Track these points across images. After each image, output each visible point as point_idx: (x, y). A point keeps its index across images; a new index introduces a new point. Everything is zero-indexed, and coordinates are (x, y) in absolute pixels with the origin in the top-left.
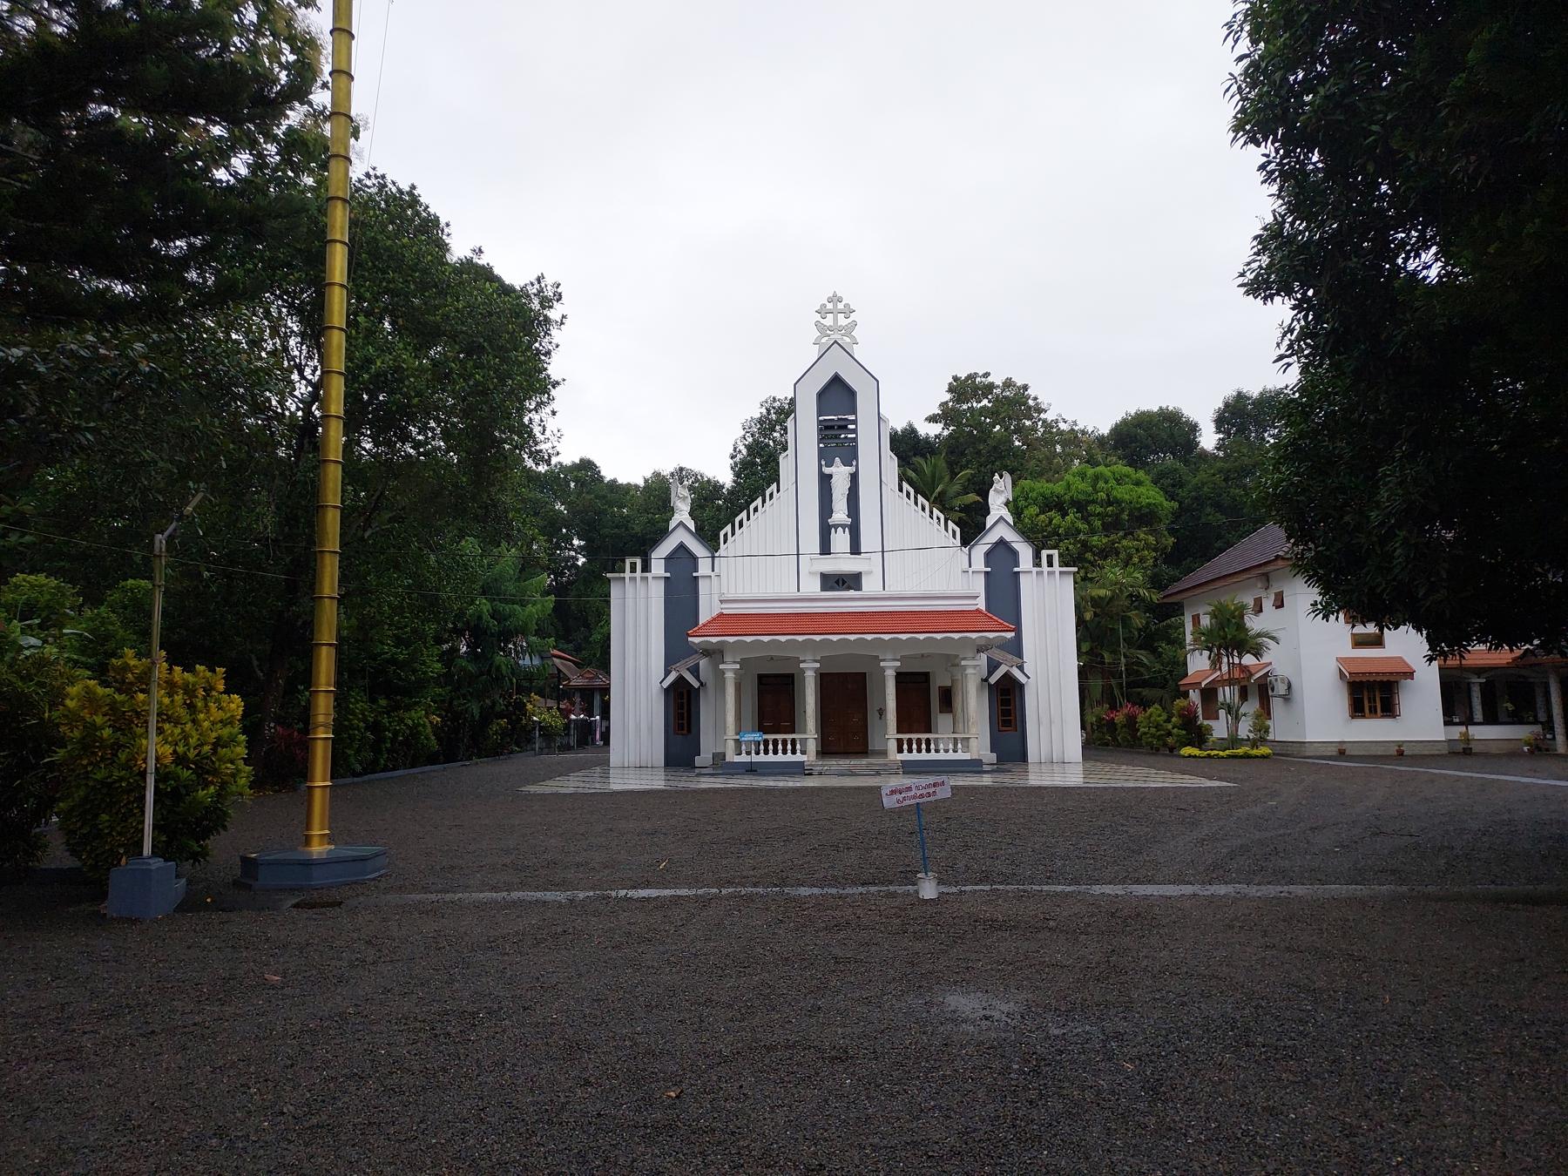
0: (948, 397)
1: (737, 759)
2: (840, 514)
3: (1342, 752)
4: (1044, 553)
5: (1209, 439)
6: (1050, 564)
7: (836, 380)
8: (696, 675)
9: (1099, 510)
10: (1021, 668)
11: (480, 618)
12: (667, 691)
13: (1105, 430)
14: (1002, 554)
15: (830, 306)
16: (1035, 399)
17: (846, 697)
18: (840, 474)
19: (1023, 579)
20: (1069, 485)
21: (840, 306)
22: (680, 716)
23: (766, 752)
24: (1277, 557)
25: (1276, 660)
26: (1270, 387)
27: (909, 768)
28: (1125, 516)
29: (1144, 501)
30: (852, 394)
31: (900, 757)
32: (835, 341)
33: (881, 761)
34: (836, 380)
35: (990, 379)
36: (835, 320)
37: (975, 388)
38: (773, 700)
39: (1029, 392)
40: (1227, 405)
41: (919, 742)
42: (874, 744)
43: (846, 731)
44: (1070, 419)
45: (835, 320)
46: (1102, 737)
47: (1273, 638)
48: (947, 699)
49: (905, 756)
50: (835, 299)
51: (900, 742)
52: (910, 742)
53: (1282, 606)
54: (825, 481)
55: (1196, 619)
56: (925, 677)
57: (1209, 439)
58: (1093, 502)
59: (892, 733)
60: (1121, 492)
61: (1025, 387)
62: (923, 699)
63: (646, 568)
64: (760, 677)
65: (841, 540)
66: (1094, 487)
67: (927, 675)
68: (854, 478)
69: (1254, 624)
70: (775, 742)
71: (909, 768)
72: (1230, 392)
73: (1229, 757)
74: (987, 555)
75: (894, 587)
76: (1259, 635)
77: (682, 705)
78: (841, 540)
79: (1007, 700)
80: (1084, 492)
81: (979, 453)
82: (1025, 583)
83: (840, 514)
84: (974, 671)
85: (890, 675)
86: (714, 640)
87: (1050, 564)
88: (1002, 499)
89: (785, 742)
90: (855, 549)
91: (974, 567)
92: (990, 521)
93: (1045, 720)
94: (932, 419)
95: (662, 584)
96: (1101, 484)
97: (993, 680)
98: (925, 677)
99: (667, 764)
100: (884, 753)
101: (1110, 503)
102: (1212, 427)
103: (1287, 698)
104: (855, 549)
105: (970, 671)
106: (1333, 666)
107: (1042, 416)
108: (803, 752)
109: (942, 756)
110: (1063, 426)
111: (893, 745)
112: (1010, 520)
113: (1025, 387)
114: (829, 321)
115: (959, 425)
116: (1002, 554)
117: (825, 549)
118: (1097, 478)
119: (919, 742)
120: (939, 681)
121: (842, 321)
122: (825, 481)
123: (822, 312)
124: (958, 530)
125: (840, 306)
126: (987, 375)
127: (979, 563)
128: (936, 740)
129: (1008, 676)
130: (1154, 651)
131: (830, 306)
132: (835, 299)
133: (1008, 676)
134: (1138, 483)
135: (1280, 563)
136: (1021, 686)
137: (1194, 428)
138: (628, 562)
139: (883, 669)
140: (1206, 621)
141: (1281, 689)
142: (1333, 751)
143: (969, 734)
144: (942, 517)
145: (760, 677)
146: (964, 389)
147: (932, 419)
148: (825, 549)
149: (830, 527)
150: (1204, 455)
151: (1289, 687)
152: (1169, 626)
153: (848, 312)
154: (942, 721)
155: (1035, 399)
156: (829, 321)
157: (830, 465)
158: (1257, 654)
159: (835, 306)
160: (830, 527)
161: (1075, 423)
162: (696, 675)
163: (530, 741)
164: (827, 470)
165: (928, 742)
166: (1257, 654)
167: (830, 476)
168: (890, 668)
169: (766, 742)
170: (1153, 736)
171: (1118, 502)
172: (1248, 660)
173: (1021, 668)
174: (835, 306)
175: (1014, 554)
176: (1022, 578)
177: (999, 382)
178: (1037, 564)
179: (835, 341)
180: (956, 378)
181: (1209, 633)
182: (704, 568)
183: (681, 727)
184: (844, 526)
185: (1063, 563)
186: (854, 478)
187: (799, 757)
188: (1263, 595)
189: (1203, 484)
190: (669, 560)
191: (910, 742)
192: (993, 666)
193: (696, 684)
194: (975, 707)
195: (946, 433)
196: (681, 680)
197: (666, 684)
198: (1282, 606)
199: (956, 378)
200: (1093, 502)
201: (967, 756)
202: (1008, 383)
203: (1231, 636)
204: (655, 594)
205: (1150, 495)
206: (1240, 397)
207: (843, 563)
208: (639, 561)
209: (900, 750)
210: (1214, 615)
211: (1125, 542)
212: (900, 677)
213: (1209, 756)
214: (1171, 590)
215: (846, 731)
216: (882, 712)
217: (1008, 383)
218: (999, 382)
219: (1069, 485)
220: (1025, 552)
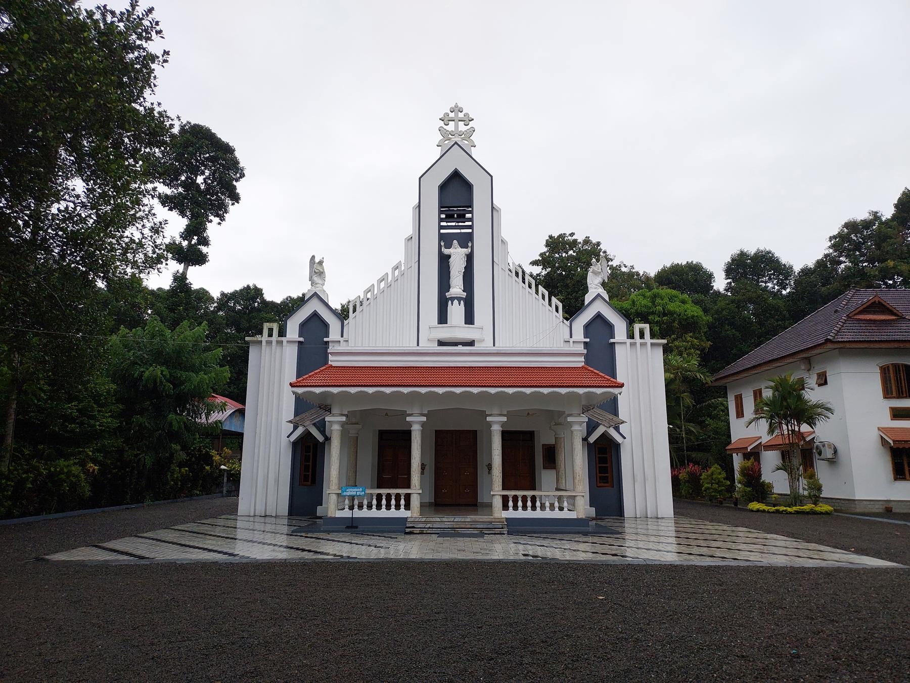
0: (545, 249)
1: (339, 514)
2: (457, 288)
3: (888, 510)
4: (637, 327)
5: (720, 283)
6: (642, 336)
7: (456, 176)
8: (322, 430)
9: (657, 319)
10: (617, 429)
11: (155, 382)
12: (295, 444)
13: (652, 273)
14: (599, 325)
15: (452, 115)
16: (605, 252)
17: (456, 450)
18: (457, 254)
19: (618, 350)
20: (633, 302)
21: (461, 115)
22: (306, 468)
23: (379, 507)
24: (828, 341)
25: (822, 432)
26: (762, 248)
27: (517, 528)
28: (676, 324)
29: (689, 313)
30: (468, 187)
31: (505, 514)
32: (456, 131)
33: (485, 518)
34: (456, 176)
35: (574, 237)
36: (457, 126)
37: (565, 243)
38: (388, 459)
39: (601, 246)
40: (733, 260)
41: (524, 499)
42: (482, 498)
43: (456, 490)
44: (629, 265)
45: (457, 126)
46: (688, 492)
47: (828, 409)
48: (551, 457)
49: (511, 514)
50: (457, 109)
51: (505, 499)
52: (515, 499)
53: (826, 383)
54: (444, 261)
55: (758, 394)
56: (530, 436)
57: (720, 283)
58: (653, 313)
59: (497, 490)
60: (671, 307)
61: (598, 244)
62: (529, 456)
63: (282, 333)
64: (382, 434)
65: (456, 311)
66: (653, 302)
67: (532, 434)
68: (470, 258)
69: (813, 395)
70: (389, 497)
71: (517, 528)
72: (735, 251)
73: (797, 512)
74: (587, 327)
75: (503, 344)
76: (817, 406)
77: (308, 456)
78: (456, 311)
79: (605, 458)
80: (645, 306)
81: (567, 286)
82: (619, 351)
83: (457, 288)
84: (578, 425)
85: (496, 429)
86: (318, 390)
87: (642, 336)
88: (599, 280)
89: (398, 497)
90: (469, 319)
91: (575, 338)
92: (588, 298)
93: (639, 478)
94: (535, 263)
95: (294, 349)
96: (658, 301)
97: (592, 439)
98: (530, 436)
99: (291, 513)
100: (489, 506)
101: (665, 314)
102: (723, 275)
103: (833, 461)
104: (469, 319)
105: (576, 428)
106: (875, 435)
107: (610, 263)
108: (408, 507)
109: (548, 514)
110: (624, 269)
111: (497, 502)
112: (606, 297)
113: (598, 244)
114: (451, 127)
115: (553, 267)
116: (599, 325)
117: (443, 318)
118: (655, 296)
119: (524, 499)
120: (544, 438)
121: (462, 127)
122: (444, 261)
123: (445, 120)
124: (560, 305)
125: (461, 115)
126: (572, 234)
127: (579, 334)
128: (541, 497)
129: (605, 437)
130: (701, 424)
131: (452, 115)
132: (457, 109)
133: (605, 437)
134: (684, 302)
135: (830, 346)
136: (617, 446)
137: (710, 276)
138: (266, 326)
139: (489, 425)
140: (768, 394)
141: (828, 453)
142: (879, 509)
143: (568, 493)
144: (546, 293)
145: (382, 434)
146: (556, 244)
147: (535, 263)
148: (443, 318)
149: (447, 300)
150: (718, 293)
151: (835, 451)
152: (710, 406)
153: (468, 120)
154: (546, 477)
155: (605, 252)
156: (451, 127)
157: (449, 246)
158: (811, 423)
159: (456, 115)
160: (447, 300)
161: (632, 267)
162: (322, 430)
163: (219, 485)
164: (446, 251)
165: (534, 499)
166: (811, 423)
167: (449, 256)
168: (497, 424)
169: (379, 497)
170: (715, 490)
171: (671, 313)
172: (805, 428)
173: (617, 429)
174: (456, 115)
175: (610, 327)
176: (617, 348)
177: (580, 240)
178: (631, 336)
179: (456, 131)
180: (551, 237)
181: (771, 403)
182: (334, 334)
183: (306, 478)
184: (459, 299)
185: (653, 336)
186: (470, 258)
187: (402, 513)
188: (805, 375)
189: (723, 310)
190: (303, 326)
191: (515, 499)
192: (592, 427)
193: (320, 438)
194: (578, 462)
195: (544, 273)
196: (307, 435)
197: (294, 437)
198: (826, 383)
199: (551, 237)
200: (653, 313)
201: (573, 515)
202: (587, 241)
203: (790, 408)
204: (289, 356)
205: (693, 310)
206: (742, 254)
207: (456, 327)
208: (275, 327)
209: (505, 507)
210: (776, 389)
211: (676, 343)
212: (506, 436)
213: (778, 511)
214: (722, 373)
215: (456, 490)
216: (490, 467)
217: (587, 241)
218: (580, 240)
219: (633, 302)
220: (620, 326)
